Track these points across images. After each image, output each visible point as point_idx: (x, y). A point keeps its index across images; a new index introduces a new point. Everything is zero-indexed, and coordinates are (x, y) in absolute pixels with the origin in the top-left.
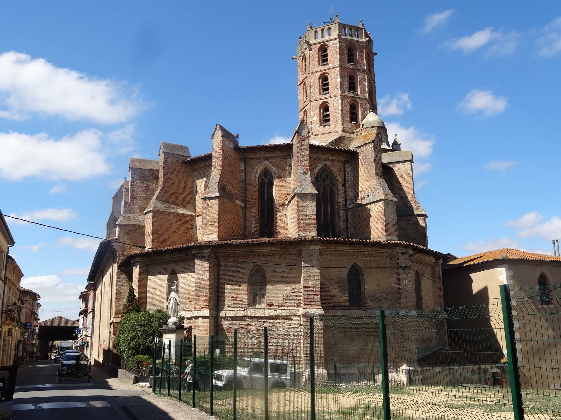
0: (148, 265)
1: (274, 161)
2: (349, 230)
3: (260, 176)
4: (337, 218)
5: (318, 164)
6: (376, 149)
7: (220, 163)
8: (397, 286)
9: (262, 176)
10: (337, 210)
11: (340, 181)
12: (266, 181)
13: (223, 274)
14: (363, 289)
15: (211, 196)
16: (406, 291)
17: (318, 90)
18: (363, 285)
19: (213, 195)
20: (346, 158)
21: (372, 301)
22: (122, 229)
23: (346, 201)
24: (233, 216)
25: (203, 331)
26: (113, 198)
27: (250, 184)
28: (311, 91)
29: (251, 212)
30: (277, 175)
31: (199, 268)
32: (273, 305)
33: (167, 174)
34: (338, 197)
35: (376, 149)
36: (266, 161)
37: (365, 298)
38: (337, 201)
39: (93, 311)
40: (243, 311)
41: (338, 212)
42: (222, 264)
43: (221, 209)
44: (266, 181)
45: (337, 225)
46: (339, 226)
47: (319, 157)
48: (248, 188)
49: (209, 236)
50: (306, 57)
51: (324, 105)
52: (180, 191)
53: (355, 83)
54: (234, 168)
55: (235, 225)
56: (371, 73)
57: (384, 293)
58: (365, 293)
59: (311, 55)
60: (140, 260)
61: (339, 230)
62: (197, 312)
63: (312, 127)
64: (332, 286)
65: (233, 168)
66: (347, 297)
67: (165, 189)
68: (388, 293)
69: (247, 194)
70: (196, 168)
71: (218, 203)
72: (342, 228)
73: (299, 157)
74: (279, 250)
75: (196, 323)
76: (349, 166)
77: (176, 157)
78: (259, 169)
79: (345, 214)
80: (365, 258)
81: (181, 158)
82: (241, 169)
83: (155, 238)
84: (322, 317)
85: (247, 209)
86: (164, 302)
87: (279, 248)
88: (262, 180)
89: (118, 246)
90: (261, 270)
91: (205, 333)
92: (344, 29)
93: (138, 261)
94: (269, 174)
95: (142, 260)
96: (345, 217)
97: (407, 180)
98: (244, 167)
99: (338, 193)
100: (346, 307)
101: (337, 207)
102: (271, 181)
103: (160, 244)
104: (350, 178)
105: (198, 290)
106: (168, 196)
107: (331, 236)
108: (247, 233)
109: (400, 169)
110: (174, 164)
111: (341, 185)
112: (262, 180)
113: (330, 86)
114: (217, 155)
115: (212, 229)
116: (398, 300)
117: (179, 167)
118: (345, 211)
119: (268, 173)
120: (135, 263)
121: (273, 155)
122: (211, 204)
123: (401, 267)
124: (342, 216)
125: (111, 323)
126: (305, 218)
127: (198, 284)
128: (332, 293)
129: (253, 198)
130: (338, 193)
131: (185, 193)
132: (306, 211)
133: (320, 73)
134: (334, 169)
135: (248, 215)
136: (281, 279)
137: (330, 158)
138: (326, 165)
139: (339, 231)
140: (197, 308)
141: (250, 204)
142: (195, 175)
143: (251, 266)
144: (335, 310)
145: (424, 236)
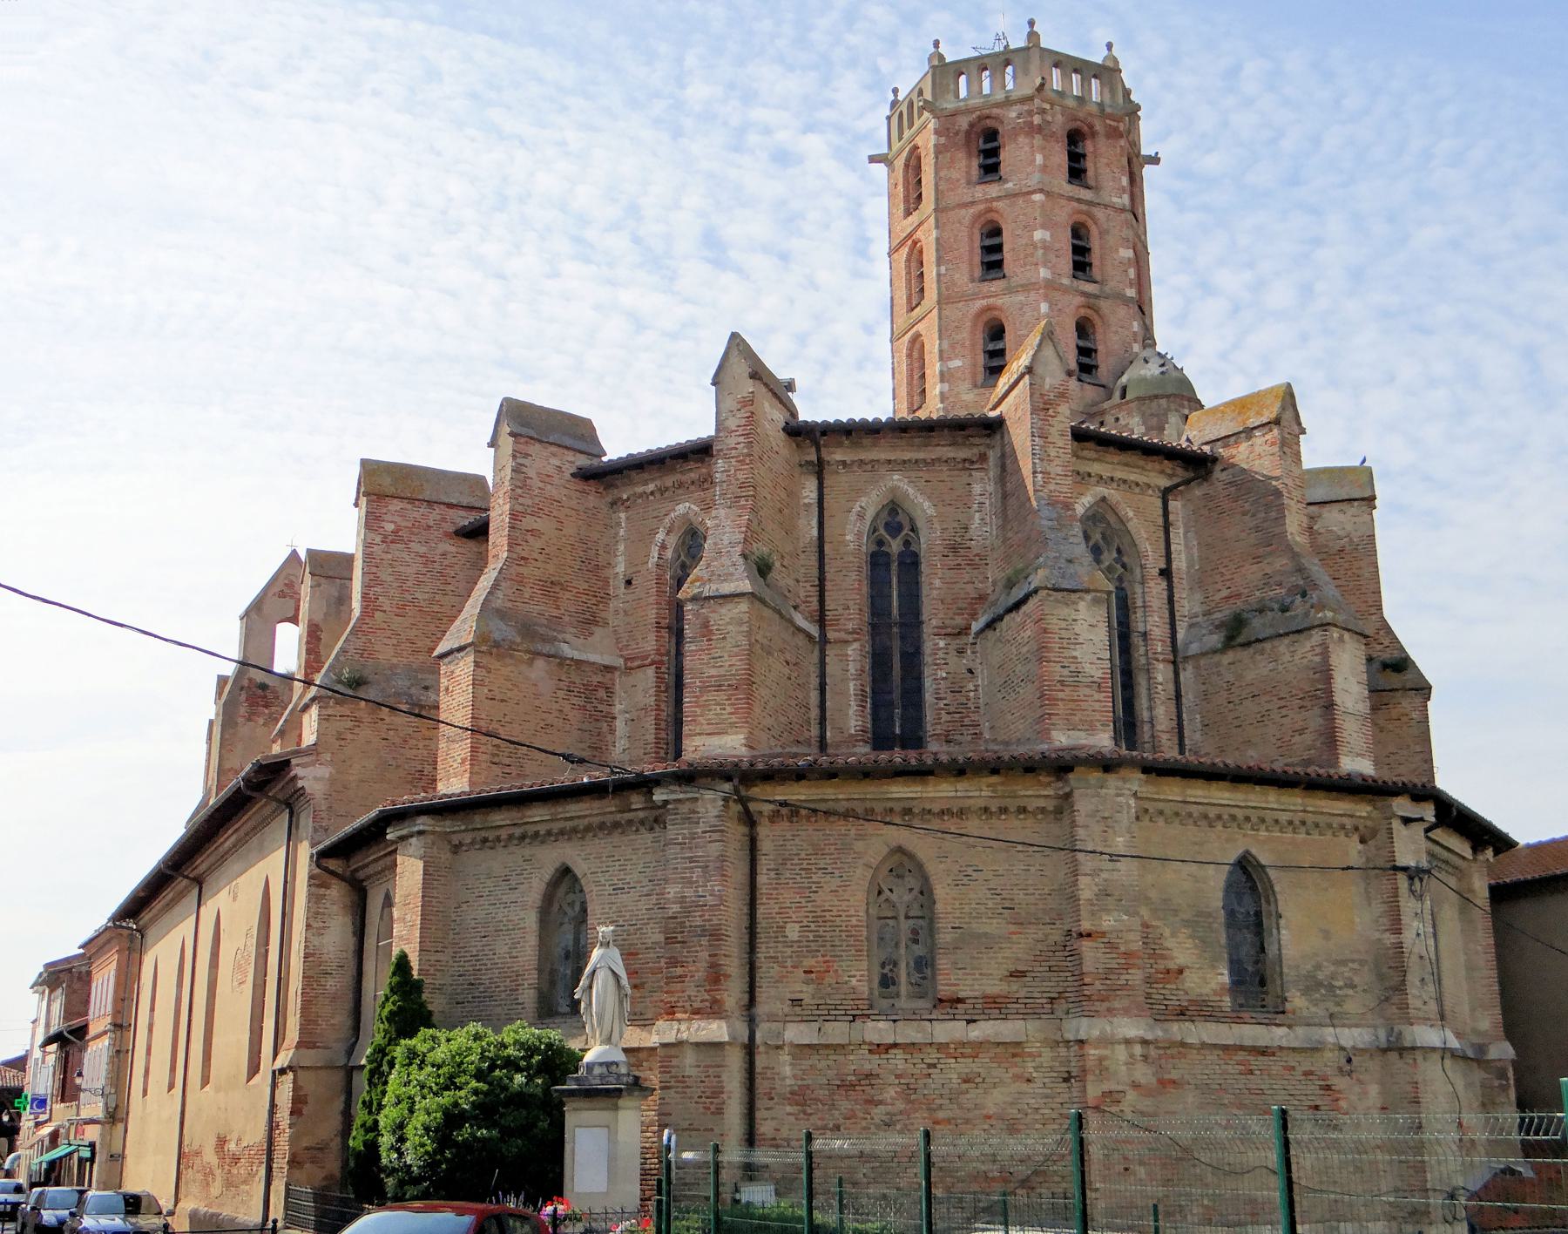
0: (456, 849)
1: (926, 476)
5: (1079, 494)
6: (1285, 449)
8: (1389, 939)
9: (882, 531)
11: (1150, 558)
12: (895, 546)
13: (771, 884)
14: (1277, 946)
15: (717, 590)
18: (1275, 931)
19: (727, 588)
20: (1170, 476)
21: (1306, 992)
22: (329, 716)
24: (786, 671)
25: (700, 1100)
26: (247, 615)
27: (838, 557)
29: (844, 658)
30: (937, 526)
31: (682, 858)
32: (960, 1000)
34: (1145, 616)
35: (1285, 449)
36: (896, 477)
37: (1282, 979)
38: (1141, 628)
39: (121, 1026)
40: (851, 1022)
41: (1148, 670)
42: (766, 845)
44: (895, 546)
48: (833, 570)
49: (715, 741)
50: (922, 156)
51: (985, 318)
52: (567, 578)
53: (1090, 249)
55: (793, 703)
56: (1137, 221)
57: (1344, 963)
58: (1281, 961)
60: (430, 828)
61: (1150, 733)
62: (675, 1025)
64: (1173, 935)
66: (1223, 974)
67: (515, 570)
68: (1355, 966)
69: (826, 594)
70: (625, 497)
73: (1037, 461)
74: (983, 794)
75: (673, 1070)
76: (1179, 506)
77: (554, 455)
78: (870, 503)
79: (1171, 675)
80: (1279, 834)
81: (573, 459)
82: (806, 501)
83: (483, 749)
86: (526, 986)
87: (985, 788)
88: (880, 543)
89: (315, 778)
90: (910, 871)
91: (709, 1109)
93: (420, 833)
95: (437, 829)
96: (1171, 687)
97: (1360, 568)
98: (814, 495)
99: (1144, 602)
100: (1223, 1014)
103: (497, 770)
104: (1183, 548)
105: (679, 942)
108: (828, 734)
109: (1335, 529)
110: (547, 479)
111: (1155, 572)
112: (880, 543)
113: (1007, 254)
114: (734, 446)
115: (722, 714)
117: (565, 491)
118: (1171, 667)
120: (402, 838)
122: (720, 622)
123: (1405, 869)
124: (1161, 684)
125: (283, 1071)
126: (1071, 679)
127: (676, 918)
128: (1172, 959)
129: (848, 608)
130: (1144, 602)
132: (1075, 654)
133: (971, 211)
135: (832, 668)
137: (1118, 475)
138: (1104, 499)
140: (675, 1009)
141: (839, 631)
142: (619, 524)
144: (1187, 1024)
145: (1426, 766)
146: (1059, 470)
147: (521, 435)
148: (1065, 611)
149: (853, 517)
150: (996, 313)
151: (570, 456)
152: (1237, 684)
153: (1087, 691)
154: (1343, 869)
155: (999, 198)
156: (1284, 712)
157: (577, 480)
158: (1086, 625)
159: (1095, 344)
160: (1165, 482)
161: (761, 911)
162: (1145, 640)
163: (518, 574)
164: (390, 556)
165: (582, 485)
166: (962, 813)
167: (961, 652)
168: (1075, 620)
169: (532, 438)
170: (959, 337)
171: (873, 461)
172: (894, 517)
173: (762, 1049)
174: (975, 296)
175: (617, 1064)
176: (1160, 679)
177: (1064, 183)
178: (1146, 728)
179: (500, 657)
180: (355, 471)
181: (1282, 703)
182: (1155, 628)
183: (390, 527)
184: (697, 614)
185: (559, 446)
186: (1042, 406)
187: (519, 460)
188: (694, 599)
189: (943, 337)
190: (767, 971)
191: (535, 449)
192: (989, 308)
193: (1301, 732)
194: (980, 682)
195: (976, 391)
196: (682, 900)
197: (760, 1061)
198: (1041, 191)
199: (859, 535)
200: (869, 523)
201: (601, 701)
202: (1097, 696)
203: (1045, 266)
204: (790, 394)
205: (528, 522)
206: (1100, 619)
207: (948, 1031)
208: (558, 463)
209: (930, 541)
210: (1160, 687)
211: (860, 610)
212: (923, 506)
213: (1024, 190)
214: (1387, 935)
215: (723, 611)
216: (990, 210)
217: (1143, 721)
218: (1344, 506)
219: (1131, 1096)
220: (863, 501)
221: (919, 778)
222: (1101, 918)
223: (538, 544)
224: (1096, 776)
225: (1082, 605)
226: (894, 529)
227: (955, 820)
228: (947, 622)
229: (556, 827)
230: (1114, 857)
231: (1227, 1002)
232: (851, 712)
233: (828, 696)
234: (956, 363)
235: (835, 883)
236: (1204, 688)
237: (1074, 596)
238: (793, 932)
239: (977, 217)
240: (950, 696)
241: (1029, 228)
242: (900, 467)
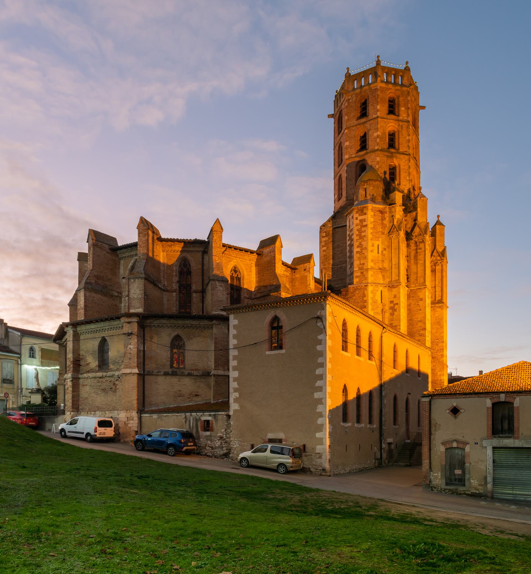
21: (113, 364)
180: (77, 254)
226: (235, 271)
231: (97, 368)
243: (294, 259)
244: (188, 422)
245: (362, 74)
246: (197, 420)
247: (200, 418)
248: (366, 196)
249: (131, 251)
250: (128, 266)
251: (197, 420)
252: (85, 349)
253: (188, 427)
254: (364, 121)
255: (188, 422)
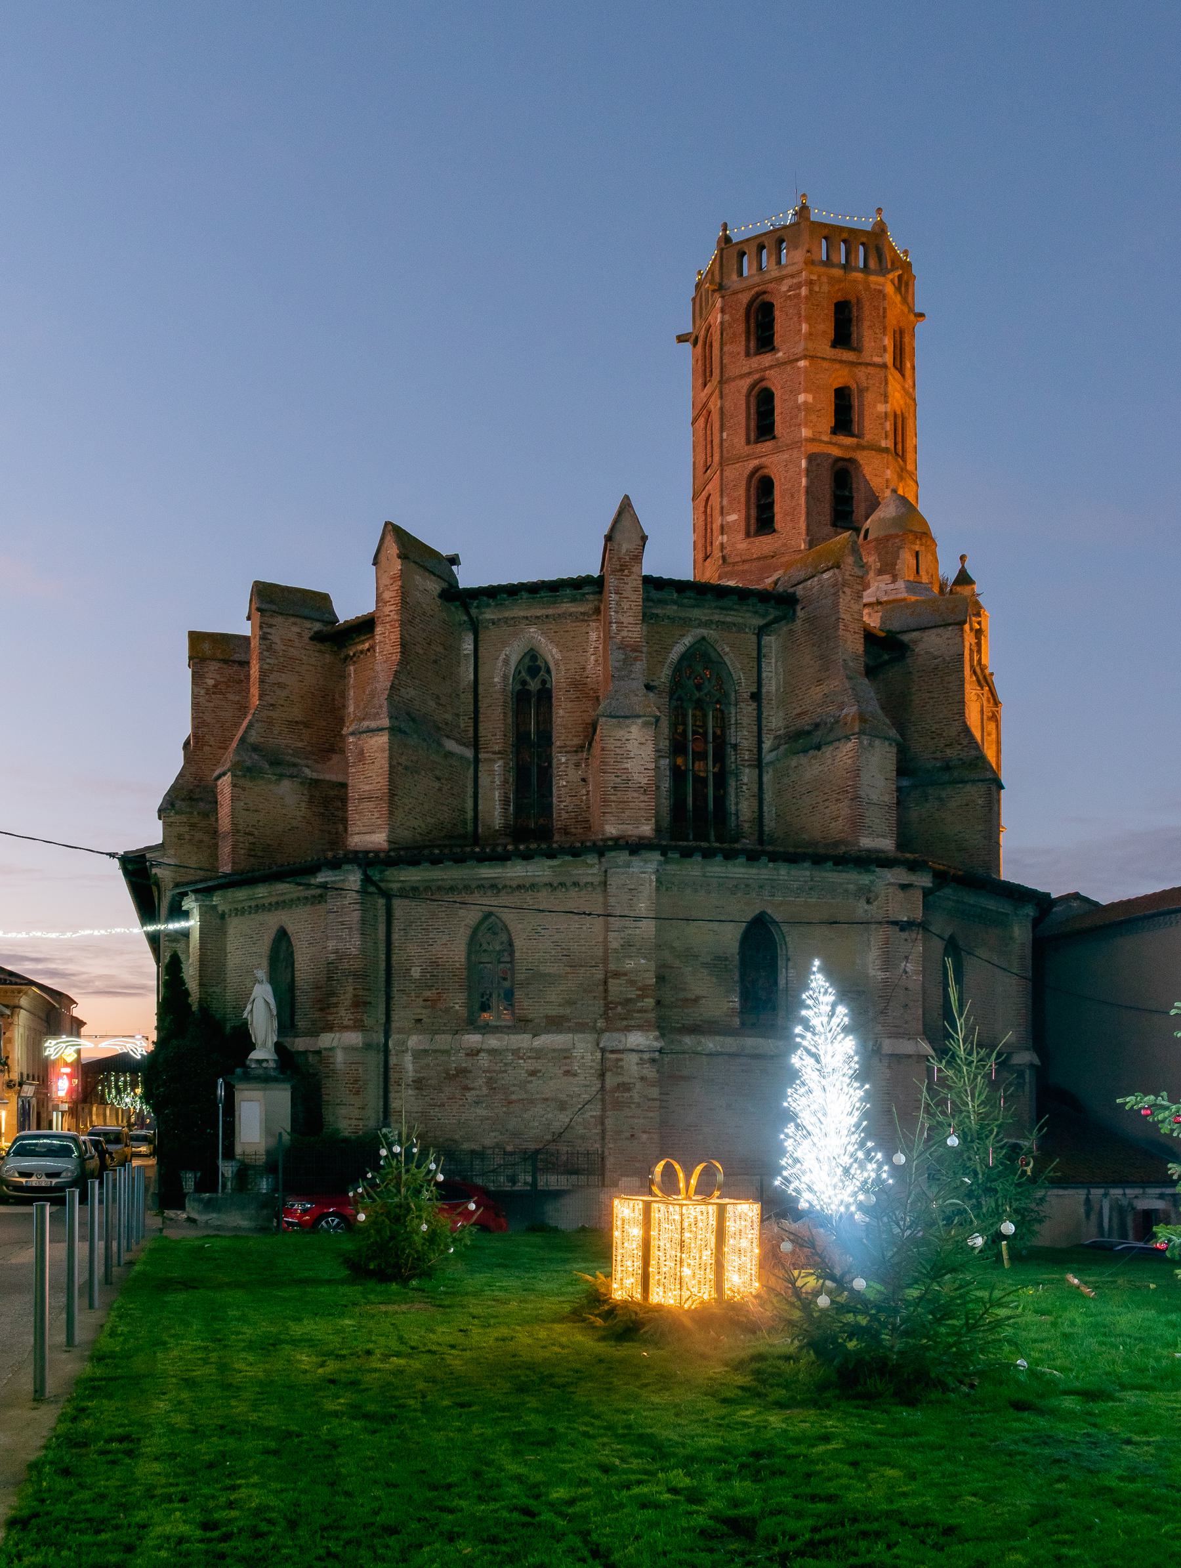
2: (766, 822)
3: (518, 672)
4: (732, 791)
7: (395, 636)
9: (523, 674)
10: (733, 766)
14: (784, 981)
16: (906, 989)
17: (742, 432)
20: (764, 616)
23: (760, 742)
24: (437, 785)
28: (725, 434)
29: (491, 772)
30: (562, 667)
33: (271, 671)
38: (733, 742)
42: (398, 913)
43: (399, 764)
45: (733, 808)
46: (737, 811)
47: (683, 614)
49: (367, 838)
54: (442, 651)
55: (445, 808)
59: (726, 324)
63: (725, 541)
65: (437, 650)
70: (351, 654)
71: (387, 746)
72: (746, 818)
77: (295, 624)
78: (514, 652)
79: (756, 777)
82: (465, 652)
84: (657, 1053)
85: (480, 765)
92: (824, 241)
94: (543, 665)
98: (471, 647)
101: (733, 758)
102: (548, 686)
106: (276, 732)
107: (713, 838)
111: (746, 696)
112: (524, 683)
116: (882, 1013)
117: (303, 652)
119: (539, 663)
121: (550, 612)
131: (324, 724)
133: (748, 381)
134: (727, 649)
135: (484, 780)
136: (553, 951)
137: (716, 618)
138: (703, 638)
139: (737, 826)
141: (487, 752)
143: (471, 916)
146: (631, 620)
147: (266, 611)
148: (620, 733)
149: (500, 663)
150: (766, 471)
151: (308, 624)
152: (799, 783)
153: (635, 795)
154: (835, 923)
155: (771, 367)
156: (827, 803)
157: (315, 642)
158: (636, 743)
159: (851, 492)
160: (759, 622)
161: (394, 958)
162: (735, 750)
163: (268, 717)
164: (212, 705)
165: (319, 646)
166: (533, 886)
167: (577, 765)
168: (628, 740)
169: (274, 612)
170: (736, 494)
171: (514, 618)
172: (533, 664)
173: (393, 1052)
174: (749, 457)
175: (267, 1061)
176: (745, 780)
177: (828, 348)
178: (733, 818)
179: (253, 779)
181: (826, 797)
182: (744, 741)
183: (211, 682)
184: (355, 744)
185: (297, 616)
186: (618, 567)
187: (266, 630)
188: (352, 734)
189: (725, 494)
190: (398, 999)
191: (278, 620)
192: (757, 469)
193: (836, 819)
194: (590, 788)
195: (748, 540)
196: (336, 952)
197: (393, 1060)
198: (805, 357)
199: (505, 677)
200: (513, 668)
201: (338, 809)
202: (643, 798)
203: (806, 426)
204: (454, 568)
205: (273, 678)
206: (647, 737)
207: (522, 1040)
208: (299, 631)
209: (559, 678)
210: (744, 787)
211: (505, 736)
212: (551, 652)
213: (792, 358)
214: (879, 973)
215: (375, 739)
216: (762, 380)
217: (731, 814)
218: (940, 630)
219: (639, 1085)
220: (507, 650)
221: (499, 862)
222: (624, 962)
223: (284, 693)
224: (623, 856)
225: (634, 729)
226: (534, 670)
227: (530, 892)
228: (567, 743)
229: (274, 900)
230: (637, 919)
231: (737, 1021)
232: (496, 813)
233: (480, 802)
234: (733, 518)
235: (445, 938)
236: (778, 786)
237: (628, 721)
238: (416, 972)
239: (753, 387)
240: (568, 799)
241: (795, 393)
242: (536, 621)
243: (325, 598)
244: (1094, 1217)
245: (845, 235)
246: (1120, 1211)
247: (1130, 1204)
248: (918, 572)
249: (693, 606)
250: (667, 649)
251: (1120, 1211)
252: (676, 944)
253: (1094, 1230)
254: (851, 359)
255: (1094, 1217)
